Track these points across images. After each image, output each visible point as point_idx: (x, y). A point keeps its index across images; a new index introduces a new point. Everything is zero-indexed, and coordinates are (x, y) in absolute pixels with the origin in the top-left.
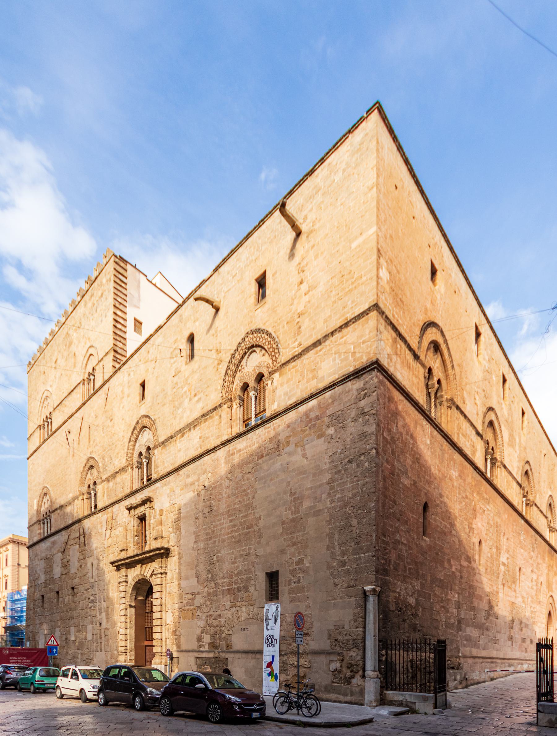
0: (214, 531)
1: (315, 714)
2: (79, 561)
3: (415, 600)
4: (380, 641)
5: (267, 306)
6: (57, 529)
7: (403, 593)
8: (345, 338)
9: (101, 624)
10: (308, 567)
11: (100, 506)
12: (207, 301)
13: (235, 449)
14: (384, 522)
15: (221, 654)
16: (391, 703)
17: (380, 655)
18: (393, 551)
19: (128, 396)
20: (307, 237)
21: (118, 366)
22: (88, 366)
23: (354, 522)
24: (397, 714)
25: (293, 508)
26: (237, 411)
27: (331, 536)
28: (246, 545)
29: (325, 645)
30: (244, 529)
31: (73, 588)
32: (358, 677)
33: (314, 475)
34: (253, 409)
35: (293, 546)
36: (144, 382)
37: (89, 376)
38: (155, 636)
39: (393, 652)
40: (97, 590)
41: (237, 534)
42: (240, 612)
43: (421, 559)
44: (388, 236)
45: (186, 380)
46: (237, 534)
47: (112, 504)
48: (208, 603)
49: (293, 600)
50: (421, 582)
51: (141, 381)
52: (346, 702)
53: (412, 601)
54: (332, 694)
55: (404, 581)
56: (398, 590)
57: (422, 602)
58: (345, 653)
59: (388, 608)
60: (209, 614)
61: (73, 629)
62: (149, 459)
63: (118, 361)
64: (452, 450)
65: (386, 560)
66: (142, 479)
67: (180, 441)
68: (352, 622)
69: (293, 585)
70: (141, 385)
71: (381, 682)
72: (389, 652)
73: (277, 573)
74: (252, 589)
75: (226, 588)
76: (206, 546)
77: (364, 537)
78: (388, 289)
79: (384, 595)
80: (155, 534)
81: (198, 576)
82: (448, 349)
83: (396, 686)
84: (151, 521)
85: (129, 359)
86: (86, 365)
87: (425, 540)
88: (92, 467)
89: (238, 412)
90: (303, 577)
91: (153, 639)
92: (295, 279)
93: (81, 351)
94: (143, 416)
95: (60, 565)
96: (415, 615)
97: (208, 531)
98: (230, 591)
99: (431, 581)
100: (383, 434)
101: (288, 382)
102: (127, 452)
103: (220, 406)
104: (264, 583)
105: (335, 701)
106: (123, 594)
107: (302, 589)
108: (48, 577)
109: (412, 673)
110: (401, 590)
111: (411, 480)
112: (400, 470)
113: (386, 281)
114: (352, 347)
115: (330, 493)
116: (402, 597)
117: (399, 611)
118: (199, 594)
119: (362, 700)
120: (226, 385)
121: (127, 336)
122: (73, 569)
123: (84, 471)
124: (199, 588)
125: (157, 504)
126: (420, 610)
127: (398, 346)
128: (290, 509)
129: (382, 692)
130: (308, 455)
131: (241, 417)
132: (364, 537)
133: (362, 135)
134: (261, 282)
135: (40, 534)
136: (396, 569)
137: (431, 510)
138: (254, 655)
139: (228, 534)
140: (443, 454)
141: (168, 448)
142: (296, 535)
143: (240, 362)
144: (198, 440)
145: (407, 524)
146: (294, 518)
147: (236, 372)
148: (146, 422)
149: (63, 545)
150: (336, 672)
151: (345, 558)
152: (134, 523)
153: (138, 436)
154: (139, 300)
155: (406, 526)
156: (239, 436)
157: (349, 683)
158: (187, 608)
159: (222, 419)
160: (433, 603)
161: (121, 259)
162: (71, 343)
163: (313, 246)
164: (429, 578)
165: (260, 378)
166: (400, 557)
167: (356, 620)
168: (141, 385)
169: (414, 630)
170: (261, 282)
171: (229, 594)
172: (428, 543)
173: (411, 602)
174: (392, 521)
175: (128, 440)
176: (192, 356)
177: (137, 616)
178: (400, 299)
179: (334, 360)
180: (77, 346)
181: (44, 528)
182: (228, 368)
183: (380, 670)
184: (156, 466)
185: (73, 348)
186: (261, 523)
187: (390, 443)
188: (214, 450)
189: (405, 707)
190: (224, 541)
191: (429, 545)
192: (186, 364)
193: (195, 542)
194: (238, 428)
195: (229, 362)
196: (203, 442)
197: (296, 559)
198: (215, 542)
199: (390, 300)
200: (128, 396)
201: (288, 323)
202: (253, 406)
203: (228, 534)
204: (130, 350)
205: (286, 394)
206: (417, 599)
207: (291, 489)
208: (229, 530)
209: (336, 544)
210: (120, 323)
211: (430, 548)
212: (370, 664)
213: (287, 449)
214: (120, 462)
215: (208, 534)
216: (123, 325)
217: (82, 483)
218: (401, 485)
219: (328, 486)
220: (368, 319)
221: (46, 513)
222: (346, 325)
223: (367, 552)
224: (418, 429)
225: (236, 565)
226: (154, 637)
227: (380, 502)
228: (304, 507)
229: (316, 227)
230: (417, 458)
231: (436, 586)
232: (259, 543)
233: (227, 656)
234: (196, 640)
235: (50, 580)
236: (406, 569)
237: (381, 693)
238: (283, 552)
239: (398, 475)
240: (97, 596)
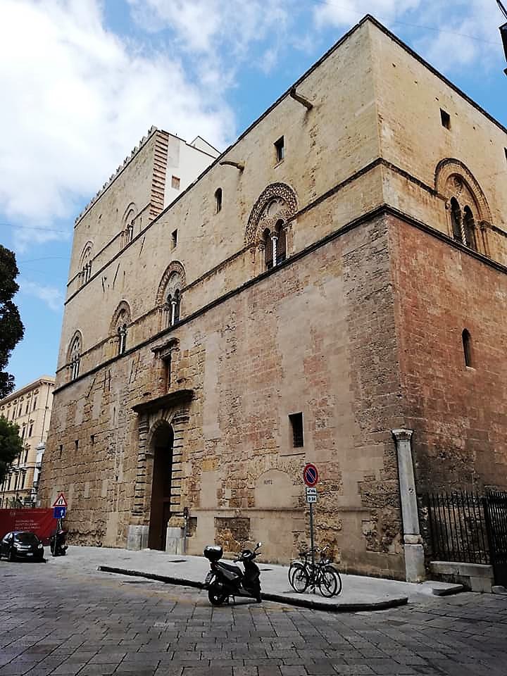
1: (334, 594)
2: (101, 407)
3: (464, 442)
4: (418, 495)
5: (284, 165)
7: (446, 434)
8: (355, 187)
9: (117, 478)
10: (332, 409)
11: (127, 349)
12: (232, 164)
13: (258, 289)
14: (410, 357)
15: (242, 512)
16: (439, 577)
17: (420, 514)
18: (425, 387)
20: (318, 110)
21: (154, 218)
23: (376, 359)
24: (443, 593)
25: (314, 346)
26: (261, 255)
27: (353, 374)
28: (268, 386)
29: (354, 500)
30: (266, 368)
31: (93, 437)
32: (395, 541)
33: (333, 312)
34: (274, 252)
35: (315, 385)
36: (176, 232)
37: (128, 228)
38: (173, 491)
39: (441, 508)
41: (260, 374)
42: (263, 461)
43: (467, 392)
45: (214, 229)
46: (260, 374)
47: (139, 347)
48: (230, 451)
49: (318, 447)
50: (471, 420)
52: (384, 577)
53: (460, 443)
54: (368, 566)
55: (445, 420)
56: (438, 432)
57: (476, 443)
58: (378, 511)
59: (426, 454)
60: (231, 464)
61: (88, 485)
62: (178, 302)
64: (493, 272)
65: (416, 398)
66: (170, 321)
67: (206, 285)
68: (384, 473)
69: (318, 430)
70: (173, 234)
71: (425, 549)
72: (432, 509)
73: (300, 414)
74: (274, 434)
75: (248, 433)
77: (388, 374)
78: (393, 143)
79: (418, 439)
80: (179, 376)
81: (220, 421)
82: (473, 178)
83: (445, 555)
84: (175, 364)
85: (164, 212)
86: (126, 218)
87: (470, 371)
88: (123, 311)
89: (261, 256)
90: (327, 420)
92: (309, 141)
93: (122, 208)
94: (173, 262)
96: (468, 460)
98: (252, 437)
99: (485, 417)
100: (399, 270)
101: (305, 228)
103: (244, 251)
104: (288, 427)
105: (371, 576)
106: (142, 443)
107: (327, 434)
109: (472, 535)
110: (441, 431)
111: (442, 310)
112: (425, 301)
113: (390, 138)
114: (362, 194)
115: (349, 330)
116: (444, 440)
117: (442, 457)
119: (403, 574)
120: (250, 231)
122: (95, 414)
123: (115, 314)
124: (220, 435)
125: (182, 346)
126: (474, 453)
127: (410, 187)
128: (311, 347)
129: (429, 563)
130: (326, 293)
131: (264, 259)
132: (388, 374)
133: (358, 36)
134: (279, 145)
135: (67, 378)
136: (431, 407)
137: (473, 337)
138: (278, 515)
139: (252, 374)
140: (481, 277)
141: (195, 290)
142: (318, 374)
143: (262, 211)
145: (442, 357)
146: (315, 357)
147: (258, 220)
148: (176, 267)
150: (370, 536)
151: (369, 399)
152: (159, 364)
153: (168, 280)
154: (178, 161)
155: (441, 358)
156: (261, 278)
157: (387, 550)
158: (208, 457)
159: (245, 262)
160: (492, 444)
161: (163, 132)
162: (114, 201)
163: (322, 117)
164: (482, 414)
165: (280, 224)
166: (435, 393)
167: (387, 470)
168: (173, 234)
169: (469, 478)
170: (279, 145)
172: (475, 373)
173: (458, 445)
174: (420, 355)
176: (219, 208)
177: (156, 467)
178: (408, 148)
179: (346, 206)
180: (120, 203)
181: (72, 373)
182: (251, 217)
183: (422, 532)
184: (183, 308)
185: (117, 205)
186: (283, 362)
187: (408, 277)
188: (238, 291)
189: (457, 583)
191: (476, 375)
192: (214, 215)
193: (219, 383)
194: (261, 270)
196: (228, 283)
197: (319, 400)
198: (237, 383)
199: (396, 151)
201: (303, 177)
202: (275, 249)
203: (252, 374)
204: (167, 202)
205: (304, 238)
206: (466, 441)
207: (311, 327)
208: (252, 371)
209: (360, 382)
210: (159, 182)
211: (478, 379)
212: (410, 522)
213: (306, 289)
214: (150, 305)
215: (231, 374)
216: (162, 184)
217: (113, 325)
218: (428, 316)
219: (347, 324)
220: (374, 171)
221: (76, 357)
222: (355, 177)
223: (393, 391)
224: (444, 257)
225: (259, 407)
226: (172, 493)
227: (403, 337)
228: (325, 346)
229: (325, 101)
230: (447, 286)
231: (494, 422)
232: (281, 383)
233: (249, 515)
234: (216, 496)
235: (72, 428)
236: (447, 406)
237: (427, 564)
238: (305, 392)
239: (423, 306)
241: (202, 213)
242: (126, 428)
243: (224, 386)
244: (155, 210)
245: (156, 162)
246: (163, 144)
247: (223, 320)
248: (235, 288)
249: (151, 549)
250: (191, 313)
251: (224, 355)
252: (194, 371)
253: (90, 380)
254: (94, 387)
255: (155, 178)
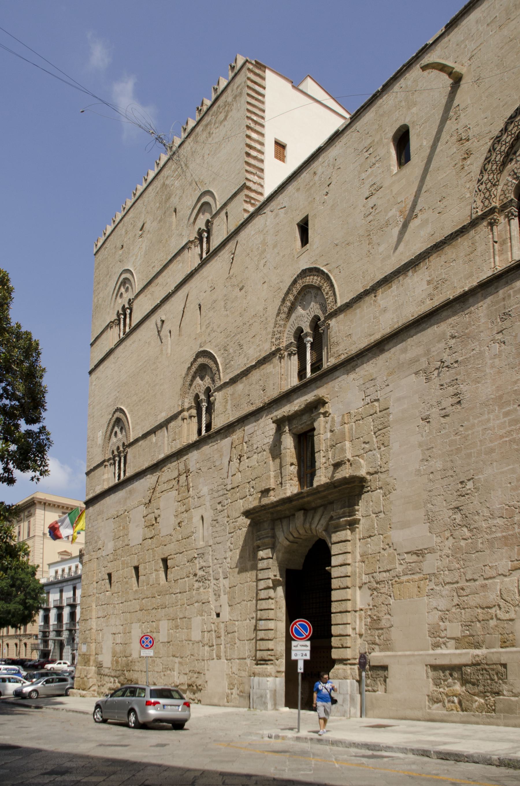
0: (466, 438)
6: (138, 470)
19: (275, 246)
21: (251, 209)
22: (198, 221)
38: (335, 630)
40: (210, 560)
44: (499, 337)
51: (299, 219)
63: (253, 201)
75: (499, 535)
76: (449, 464)
81: (430, 520)
86: (195, 219)
91: (332, 636)
95: (142, 523)
97: (453, 438)
102: (274, 332)
108: (120, 543)
118: (432, 551)
121: (266, 166)
144: (425, 286)
149: (149, 494)
171: (506, 546)
175: (276, 312)
190: (492, 451)
195: (490, 151)
198: (469, 456)
200: (275, 246)
221: (118, 448)
240: (210, 570)
241: (364, 176)
242: (228, 544)
243: (438, 464)
244: (253, 195)
245: (249, 115)
246: (255, 83)
247: (428, 352)
248: (451, 295)
249: (290, 708)
250: (354, 350)
251: (435, 412)
252: (367, 446)
253: (149, 480)
254: (159, 489)
255: (248, 141)
